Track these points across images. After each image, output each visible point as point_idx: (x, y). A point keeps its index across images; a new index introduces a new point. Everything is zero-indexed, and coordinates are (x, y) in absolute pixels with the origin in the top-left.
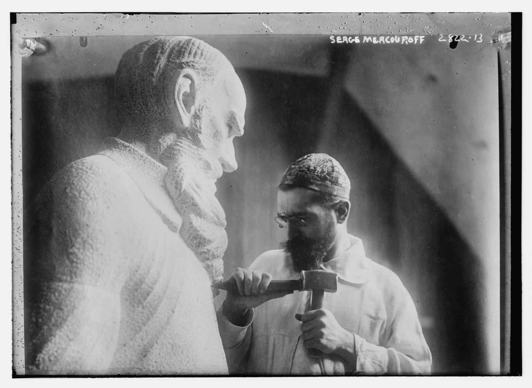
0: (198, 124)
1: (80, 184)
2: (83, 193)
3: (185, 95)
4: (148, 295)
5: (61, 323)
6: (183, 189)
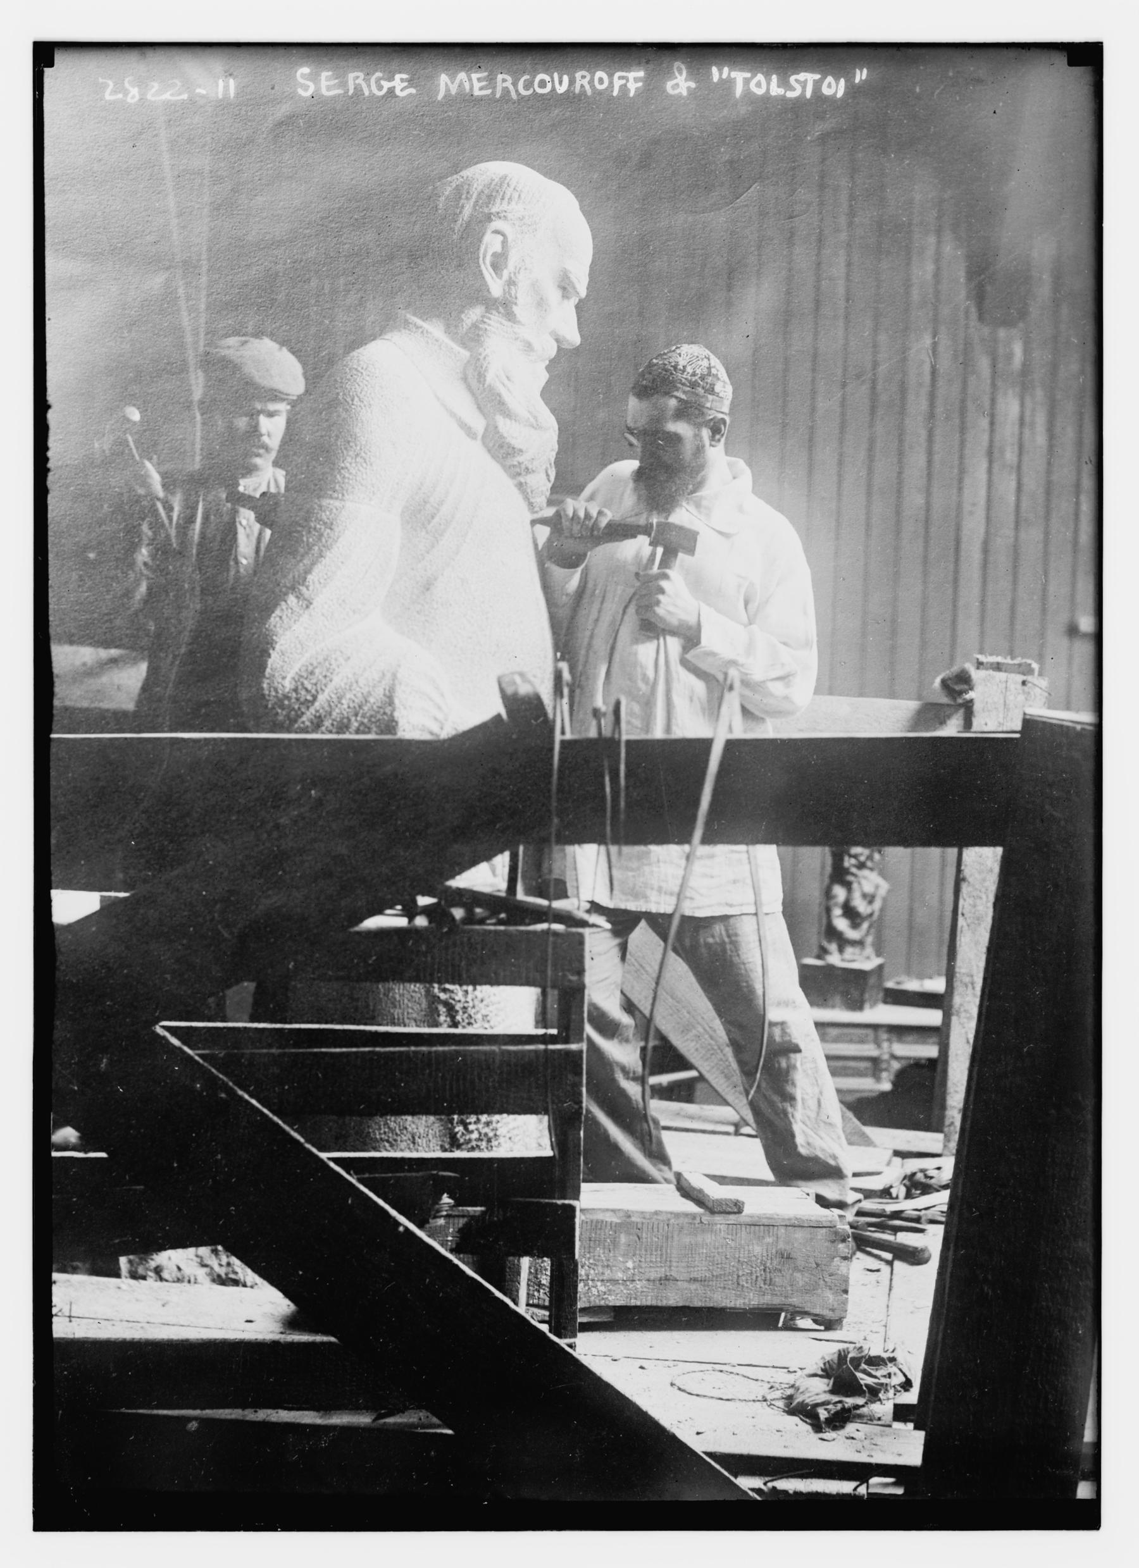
0: (513, 292)
1: (353, 388)
2: (356, 399)
3: (494, 255)
4: (433, 517)
5: (331, 545)
6: (487, 383)
